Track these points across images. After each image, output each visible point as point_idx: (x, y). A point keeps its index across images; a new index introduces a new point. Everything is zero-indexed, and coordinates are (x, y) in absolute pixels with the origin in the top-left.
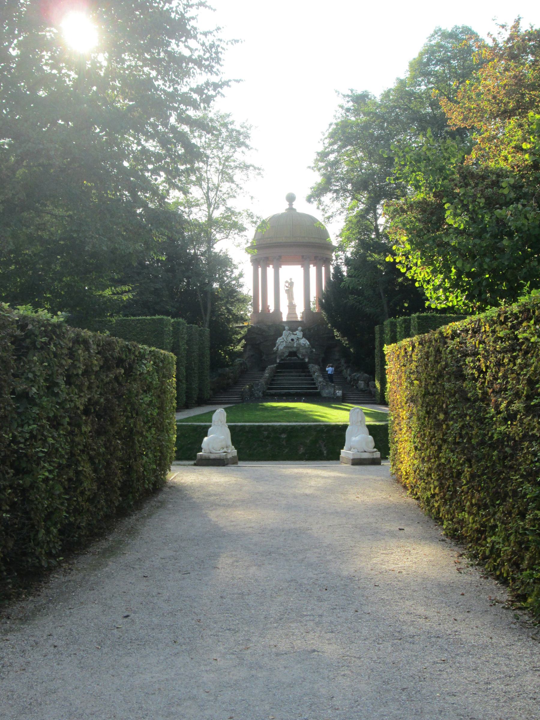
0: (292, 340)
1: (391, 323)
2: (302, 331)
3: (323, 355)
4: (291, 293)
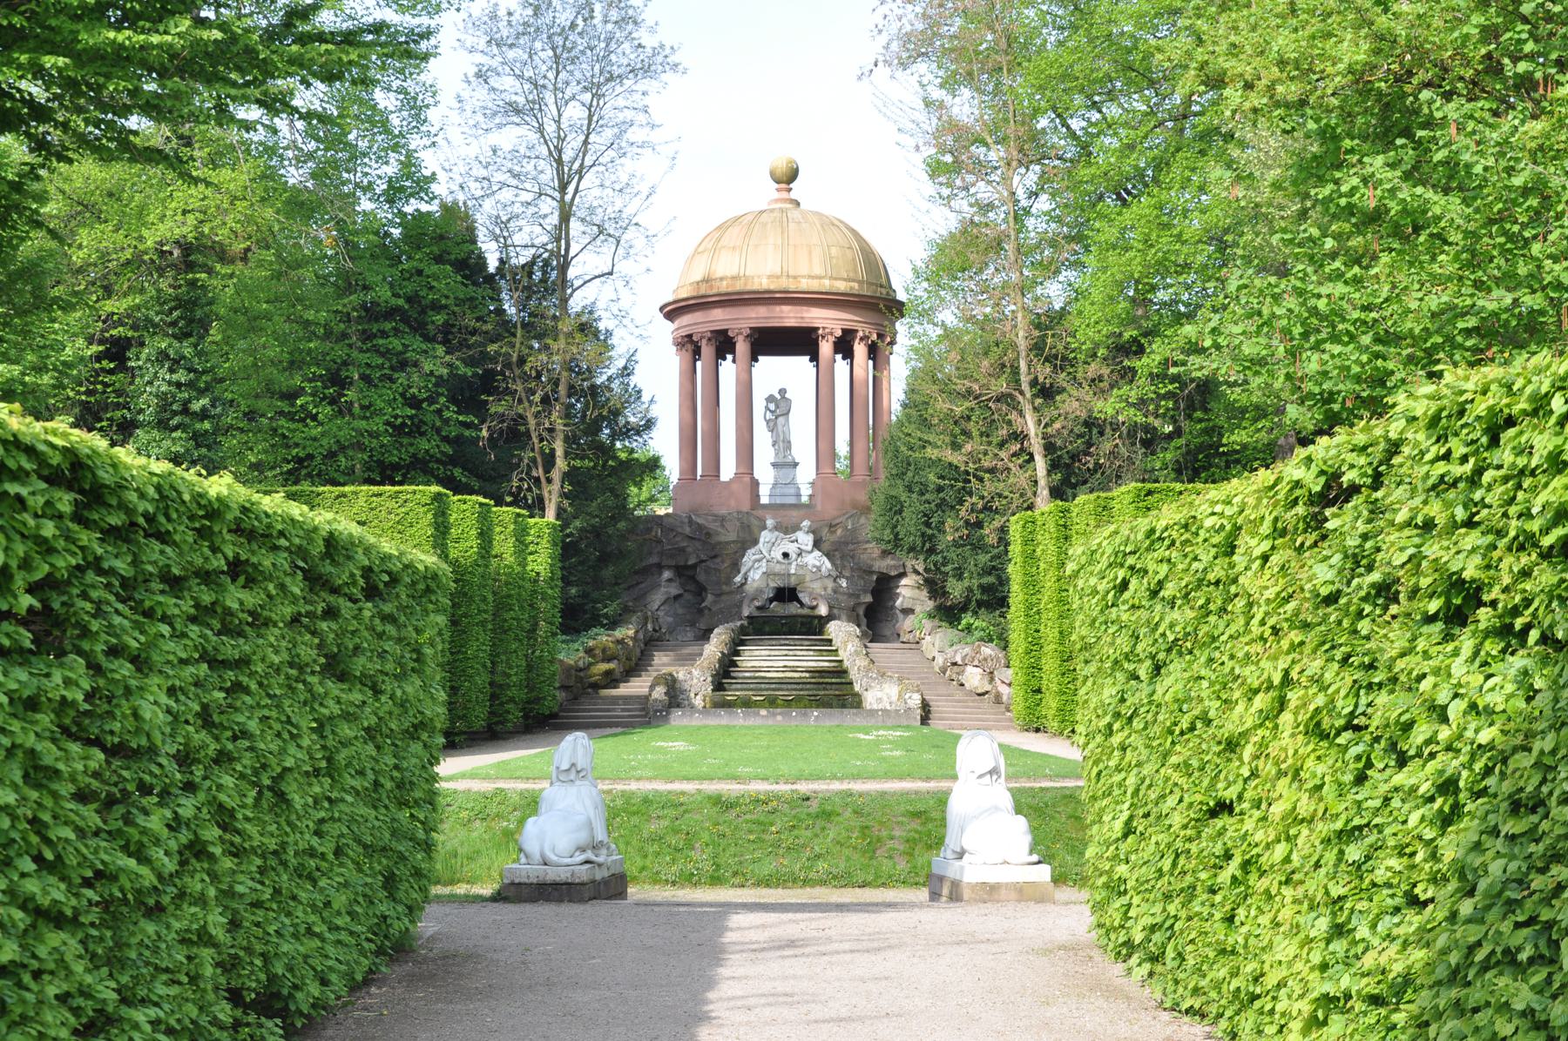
2: (813, 531)
3: (869, 599)
4: (790, 436)
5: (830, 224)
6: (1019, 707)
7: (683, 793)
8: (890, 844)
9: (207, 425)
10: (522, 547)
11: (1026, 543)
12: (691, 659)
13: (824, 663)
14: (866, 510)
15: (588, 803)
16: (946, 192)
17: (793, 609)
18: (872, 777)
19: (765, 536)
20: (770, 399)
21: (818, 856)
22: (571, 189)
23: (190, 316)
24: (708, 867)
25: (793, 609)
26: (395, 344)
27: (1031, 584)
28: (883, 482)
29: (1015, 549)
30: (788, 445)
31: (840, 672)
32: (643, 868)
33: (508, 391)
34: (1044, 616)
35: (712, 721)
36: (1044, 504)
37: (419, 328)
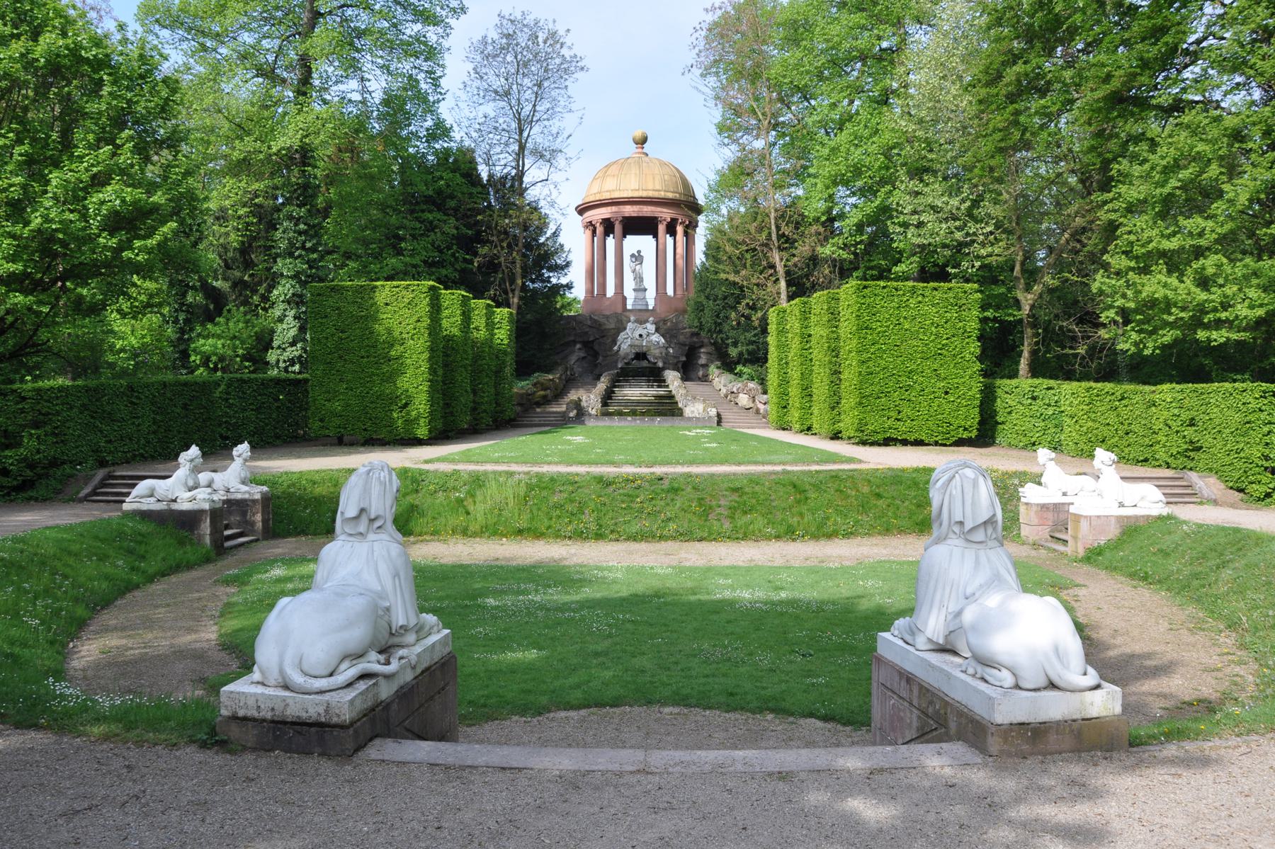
3: (684, 359)
4: (644, 275)
5: (663, 164)
6: (773, 416)
7: (577, 475)
8: (718, 510)
9: (315, 256)
10: (490, 325)
11: (779, 324)
12: (589, 391)
13: (662, 391)
14: (685, 311)
15: (383, 568)
16: (726, 141)
17: (645, 364)
18: (703, 463)
19: (630, 325)
20: (633, 256)
21: (670, 519)
22: (525, 134)
23: (305, 193)
24: (593, 527)
25: (645, 364)
26: (430, 216)
27: (783, 347)
28: (692, 295)
29: (772, 328)
30: (641, 280)
31: (671, 397)
32: (549, 527)
33: (488, 241)
34: (791, 364)
35: (601, 424)
36: (784, 304)
37: (440, 207)
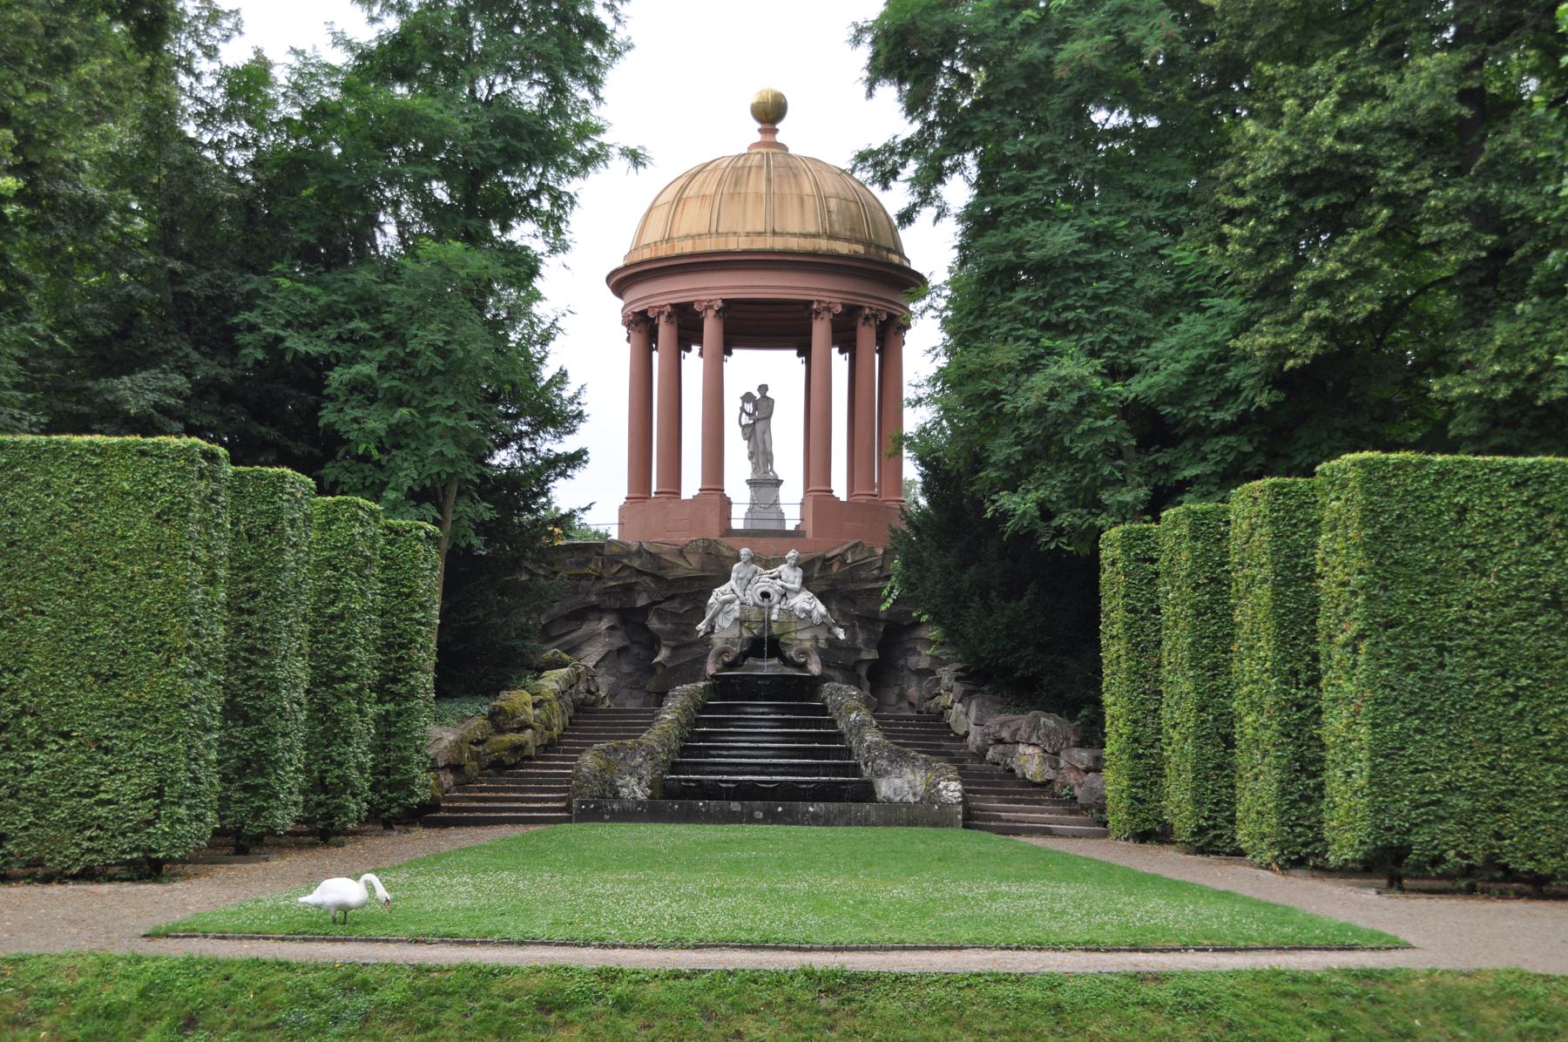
0: (765, 595)
1: (1198, 520)
20: (747, 397)
